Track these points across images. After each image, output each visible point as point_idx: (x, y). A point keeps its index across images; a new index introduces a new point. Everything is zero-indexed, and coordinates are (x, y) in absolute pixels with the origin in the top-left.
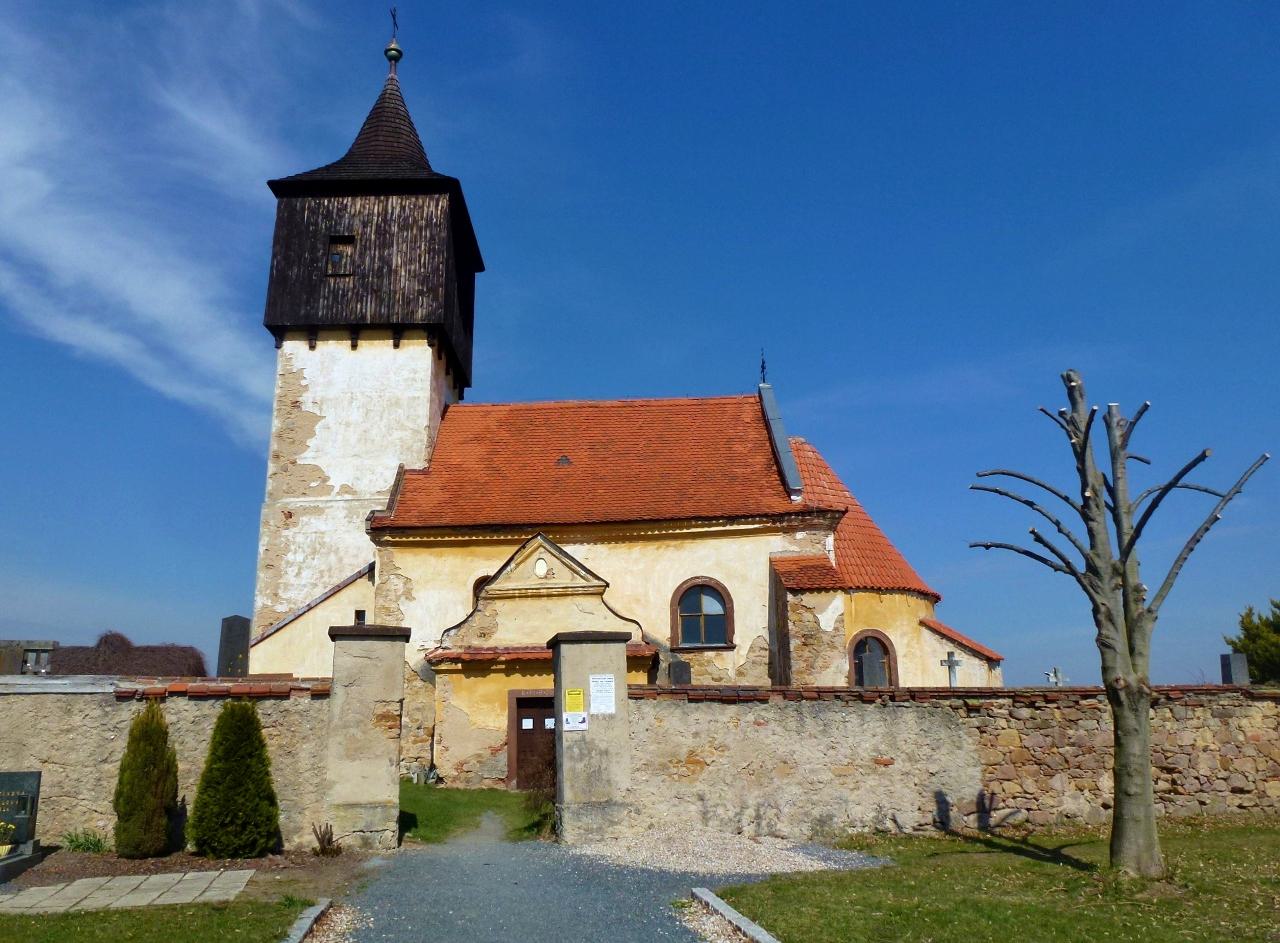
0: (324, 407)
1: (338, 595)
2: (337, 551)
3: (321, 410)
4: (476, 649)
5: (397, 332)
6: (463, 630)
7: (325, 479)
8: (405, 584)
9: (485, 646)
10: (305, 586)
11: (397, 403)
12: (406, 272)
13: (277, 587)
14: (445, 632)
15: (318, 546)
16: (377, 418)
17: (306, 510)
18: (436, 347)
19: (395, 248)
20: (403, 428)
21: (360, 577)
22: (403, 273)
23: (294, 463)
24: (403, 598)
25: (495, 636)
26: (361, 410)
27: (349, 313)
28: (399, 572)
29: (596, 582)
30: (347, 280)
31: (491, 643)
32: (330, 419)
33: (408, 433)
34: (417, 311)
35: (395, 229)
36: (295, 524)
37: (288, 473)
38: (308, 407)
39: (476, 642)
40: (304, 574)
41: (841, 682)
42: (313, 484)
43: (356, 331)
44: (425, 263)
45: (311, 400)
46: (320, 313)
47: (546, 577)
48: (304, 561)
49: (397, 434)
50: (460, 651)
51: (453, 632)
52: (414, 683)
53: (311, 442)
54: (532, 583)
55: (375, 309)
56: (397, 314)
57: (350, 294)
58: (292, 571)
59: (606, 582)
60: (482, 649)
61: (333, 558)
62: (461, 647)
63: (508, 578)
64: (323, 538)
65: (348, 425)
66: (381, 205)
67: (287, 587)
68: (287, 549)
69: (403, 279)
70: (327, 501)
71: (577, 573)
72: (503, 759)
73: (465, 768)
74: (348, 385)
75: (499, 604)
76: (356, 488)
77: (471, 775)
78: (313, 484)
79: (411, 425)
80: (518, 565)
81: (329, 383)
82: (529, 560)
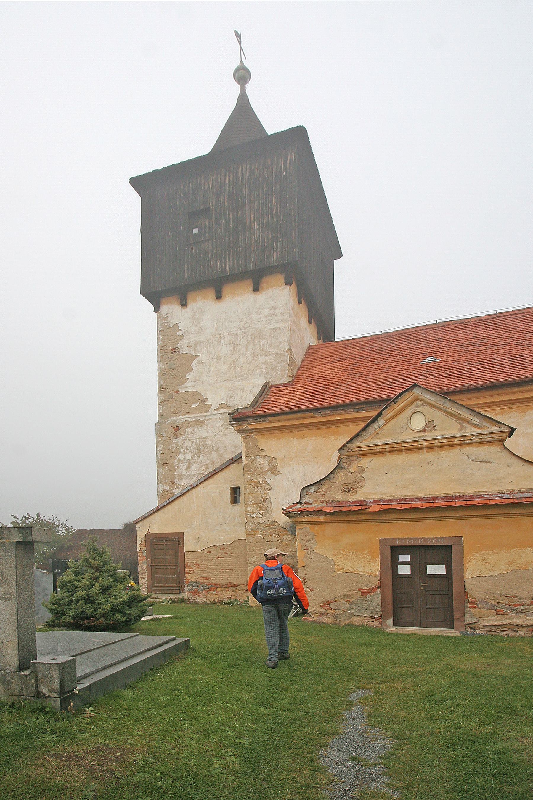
0: (198, 348)
1: (215, 477)
2: (218, 450)
3: (195, 351)
4: (339, 502)
5: (256, 280)
6: (324, 487)
7: (204, 400)
8: (270, 462)
9: (351, 500)
10: (194, 475)
11: (260, 335)
12: (259, 225)
13: (173, 477)
14: (304, 488)
15: (202, 448)
16: (244, 350)
17: (189, 424)
18: (294, 285)
19: (247, 209)
20: (267, 354)
21: (233, 463)
22: (257, 227)
23: (178, 392)
24: (269, 473)
25: (363, 490)
26: (229, 345)
27: (210, 271)
28: (264, 453)
29: (495, 429)
30: (202, 245)
31: (358, 497)
32: (203, 355)
33: (272, 357)
34: (273, 256)
35: (246, 191)
36: (183, 434)
37: (174, 400)
38: (185, 350)
39: (339, 497)
40: (193, 468)
41: (38, 634)
42: (194, 405)
43: (218, 286)
44: (277, 212)
45: (186, 345)
46: (186, 276)
47: (424, 430)
48: (192, 459)
49: (261, 360)
50: (321, 505)
51: (312, 489)
52: (284, 537)
53: (190, 376)
54: (409, 437)
55: (233, 262)
56: (254, 261)
57: (210, 255)
58: (183, 467)
59: (511, 428)
60: (347, 502)
61: (214, 455)
62: (322, 502)
63: (376, 435)
64: (205, 441)
65: (219, 358)
66: (231, 176)
67: (180, 477)
68: (178, 452)
69: (257, 232)
70: (206, 416)
71: (468, 422)
72: (376, 599)
73: (332, 606)
74: (217, 330)
75: (365, 462)
76: (228, 404)
77: (338, 612)
78: (194, 405)
79: (275, 351)
80: (387, 421)
81: (201, 330)
82: (402, 416)
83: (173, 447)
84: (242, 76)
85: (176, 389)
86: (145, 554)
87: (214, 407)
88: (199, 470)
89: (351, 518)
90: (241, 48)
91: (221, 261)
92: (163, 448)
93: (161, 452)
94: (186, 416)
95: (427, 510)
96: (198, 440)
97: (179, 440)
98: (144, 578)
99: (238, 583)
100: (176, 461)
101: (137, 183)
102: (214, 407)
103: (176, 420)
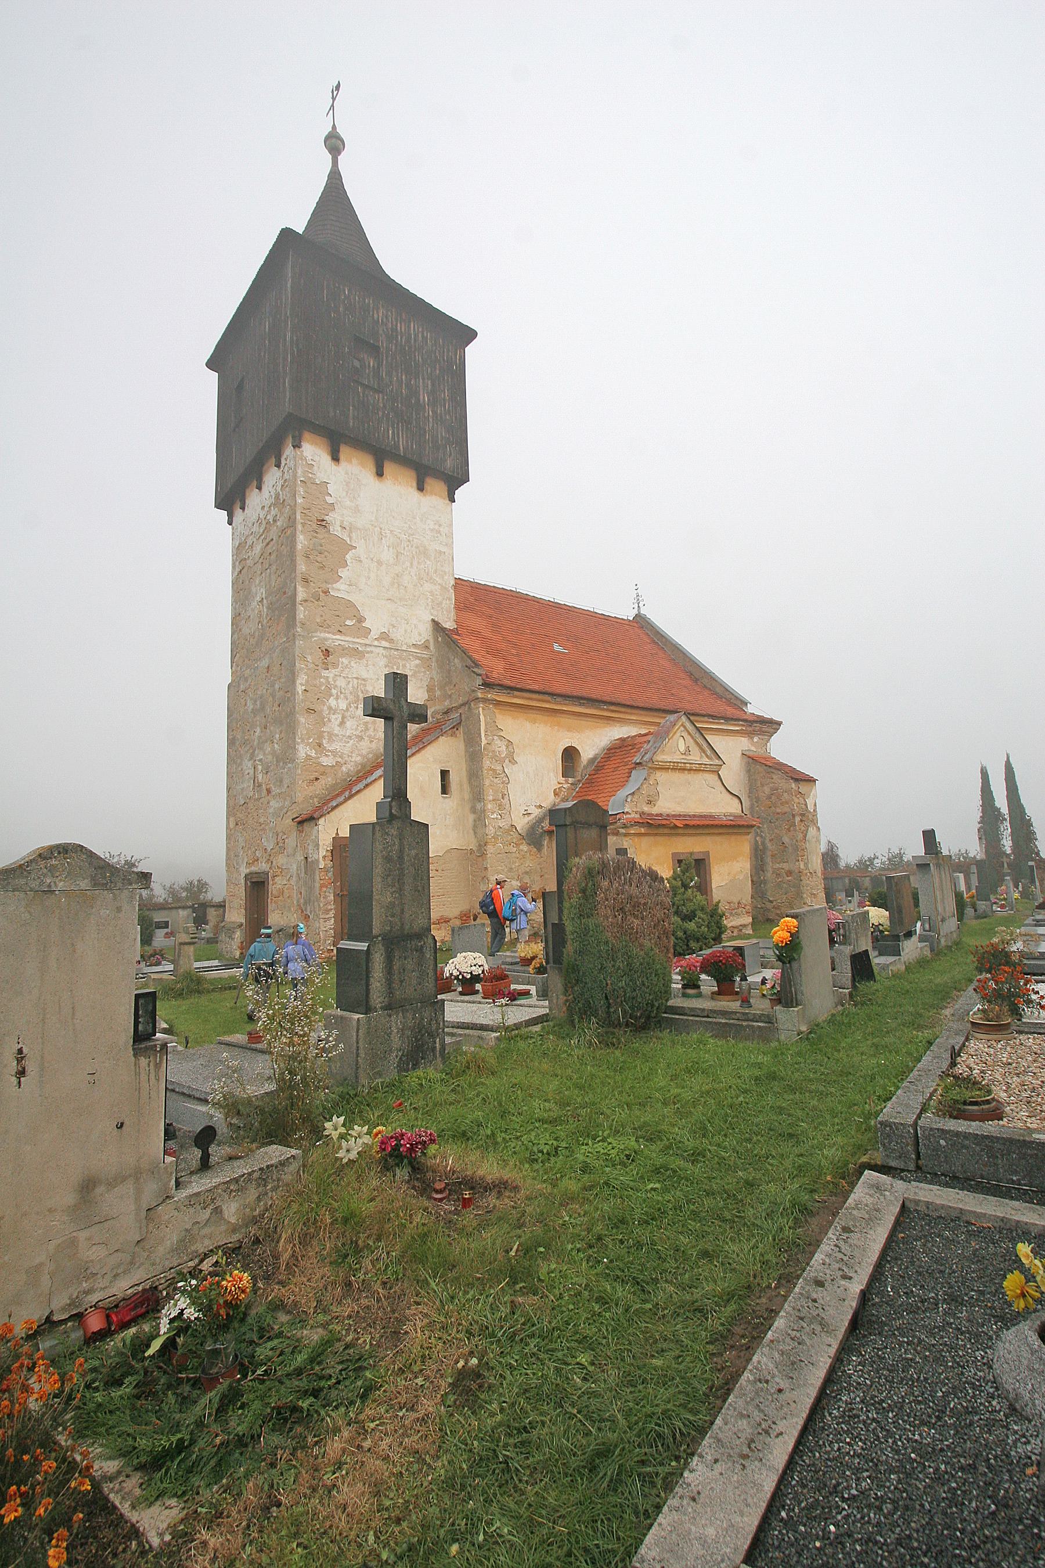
7: (361, 620)
13: (321, 736)
23: (326, 592)
32: (361, 550)
36: (335, 665)
38: (336, 530)
40: (348, 724)
48: (347, 709)
53: (343, 573)
58: (336, 719)
76: (392, 636)
83: (321, 684)
84: (334, 144)
85: (324, 586)
86: (330, 874)
87: (374, 634)
88: (356, 729)
89: (661, 831)
90: (333, 105)
91: (393, 428)
92: (307, 681)
94: (338, 637)
95: (698, 826)
96: (355, 681)
97: (330, 674)
98: (329, 919)
99: (451, 916)
100: (325, 708)
102: (374, 634)
103: (326, 639)
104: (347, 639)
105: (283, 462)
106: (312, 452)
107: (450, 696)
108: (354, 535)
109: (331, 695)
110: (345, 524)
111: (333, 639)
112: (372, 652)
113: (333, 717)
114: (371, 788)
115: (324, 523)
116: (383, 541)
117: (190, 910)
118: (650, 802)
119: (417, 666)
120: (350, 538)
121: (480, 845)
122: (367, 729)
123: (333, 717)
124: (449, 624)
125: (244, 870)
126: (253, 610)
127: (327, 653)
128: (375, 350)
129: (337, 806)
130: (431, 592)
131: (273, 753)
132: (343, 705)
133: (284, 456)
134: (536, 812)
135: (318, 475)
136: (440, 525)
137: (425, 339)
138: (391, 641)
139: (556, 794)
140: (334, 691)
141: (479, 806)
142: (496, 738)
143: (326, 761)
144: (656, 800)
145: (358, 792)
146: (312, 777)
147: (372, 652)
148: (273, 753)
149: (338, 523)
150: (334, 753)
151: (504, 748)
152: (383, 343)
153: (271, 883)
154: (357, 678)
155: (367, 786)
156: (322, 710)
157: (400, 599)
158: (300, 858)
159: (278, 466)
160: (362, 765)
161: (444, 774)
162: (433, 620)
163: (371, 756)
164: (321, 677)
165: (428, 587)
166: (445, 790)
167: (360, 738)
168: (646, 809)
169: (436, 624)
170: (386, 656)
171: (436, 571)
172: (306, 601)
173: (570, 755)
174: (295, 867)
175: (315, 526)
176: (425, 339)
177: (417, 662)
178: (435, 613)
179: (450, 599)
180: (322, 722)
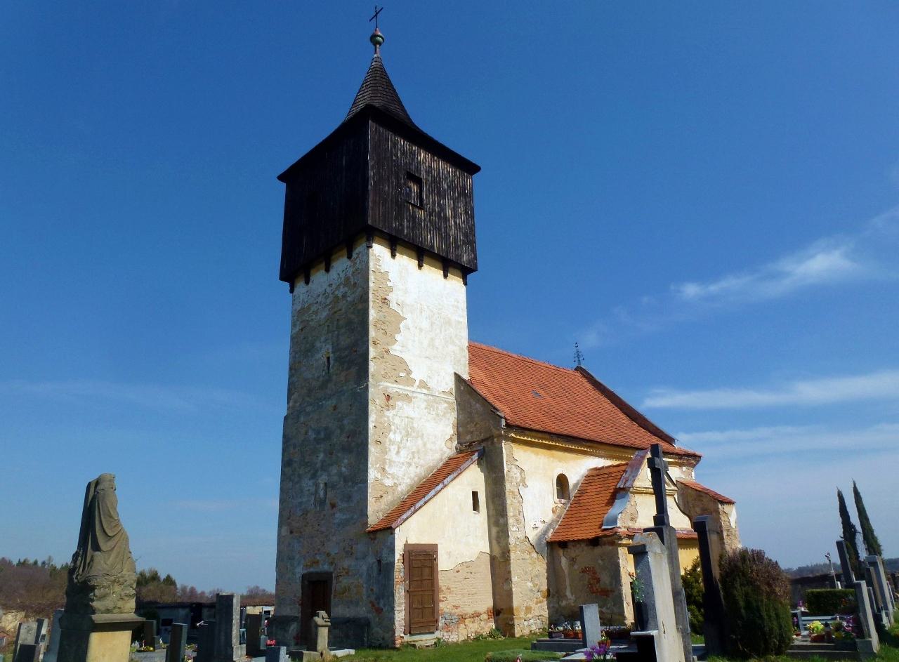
7: (409, 372)
13: (384, 463)
15: (410, 430)
23: (387, 352)
32: (409, 322)
36: (394, 407)
38: (393, 306)
58: (394, 449)
76: (429, 385)
93: (374, 424)
96: (406, 419)
97: (390, 414)
98: (401, 611)
100: (387, 440)
101: (281, 178)
103: (387, 387)
104: (401, 387)
105: (354, 255)
106: (379, 251)
107: (472, 432)
108: (404, 310)
109: (390, 431)
110: (400, 302)
111: (392, 388)
112: (416, 397)
113: (392, 447)
114: (427, 504)
115: (386, 301)
116: (423, 314)
117: (187, 610)
118: (632, 519)
119: (445, 408)
120: (402, 311)
121: (503, 553)
122: (414, 457)
123: (392, 447)
124: (466, 376)
125: (300, 571)
126: (317, 360)
127: (388, 397)
128: (418, 181)
129: (407, 518)
130: (454, 352)
131: (340, 474)
132: (398, 439)
133: (357, 251)
134: (542, 527)
135: (383, 266)
136: (458, 302)
137: (448, 172)
138: (429, 389)
139: (553, 512)
140: (393, 427)
141: (501, 521)
142: (513, 466)
143: (388, 482)
144: (637, 518)
145: (420, 508)
146: (378, 496)
147: (416, 397)
148: (340, 474)
149: (395, 302)
150: (393, 476)
151: (519, 474)
152: (423, 175)
153: (334, 582)
154: (408, 417)
155: (426, 503)
156: (385, 442)
157: (434, 357)
158: (371, 560)
159: (350, 257)
160: (410, 485)
161: (475, 494)
162: (455, 374)
163: (416, 479)
164: (385, 416)
165: (451, 348)
166: (476, 507)
167: (410, 464)
168: (631, 524)
169: (458, 378)
170: (425, 401)
171: (456, 335)
172: (375, 358)
173: (562, 481)
174: (365, 568)
175: (381, 303)
176: (448, 172)
177: (446, 405)
178: (456, 368)
179: (465, 357)
180: (384, 452)
